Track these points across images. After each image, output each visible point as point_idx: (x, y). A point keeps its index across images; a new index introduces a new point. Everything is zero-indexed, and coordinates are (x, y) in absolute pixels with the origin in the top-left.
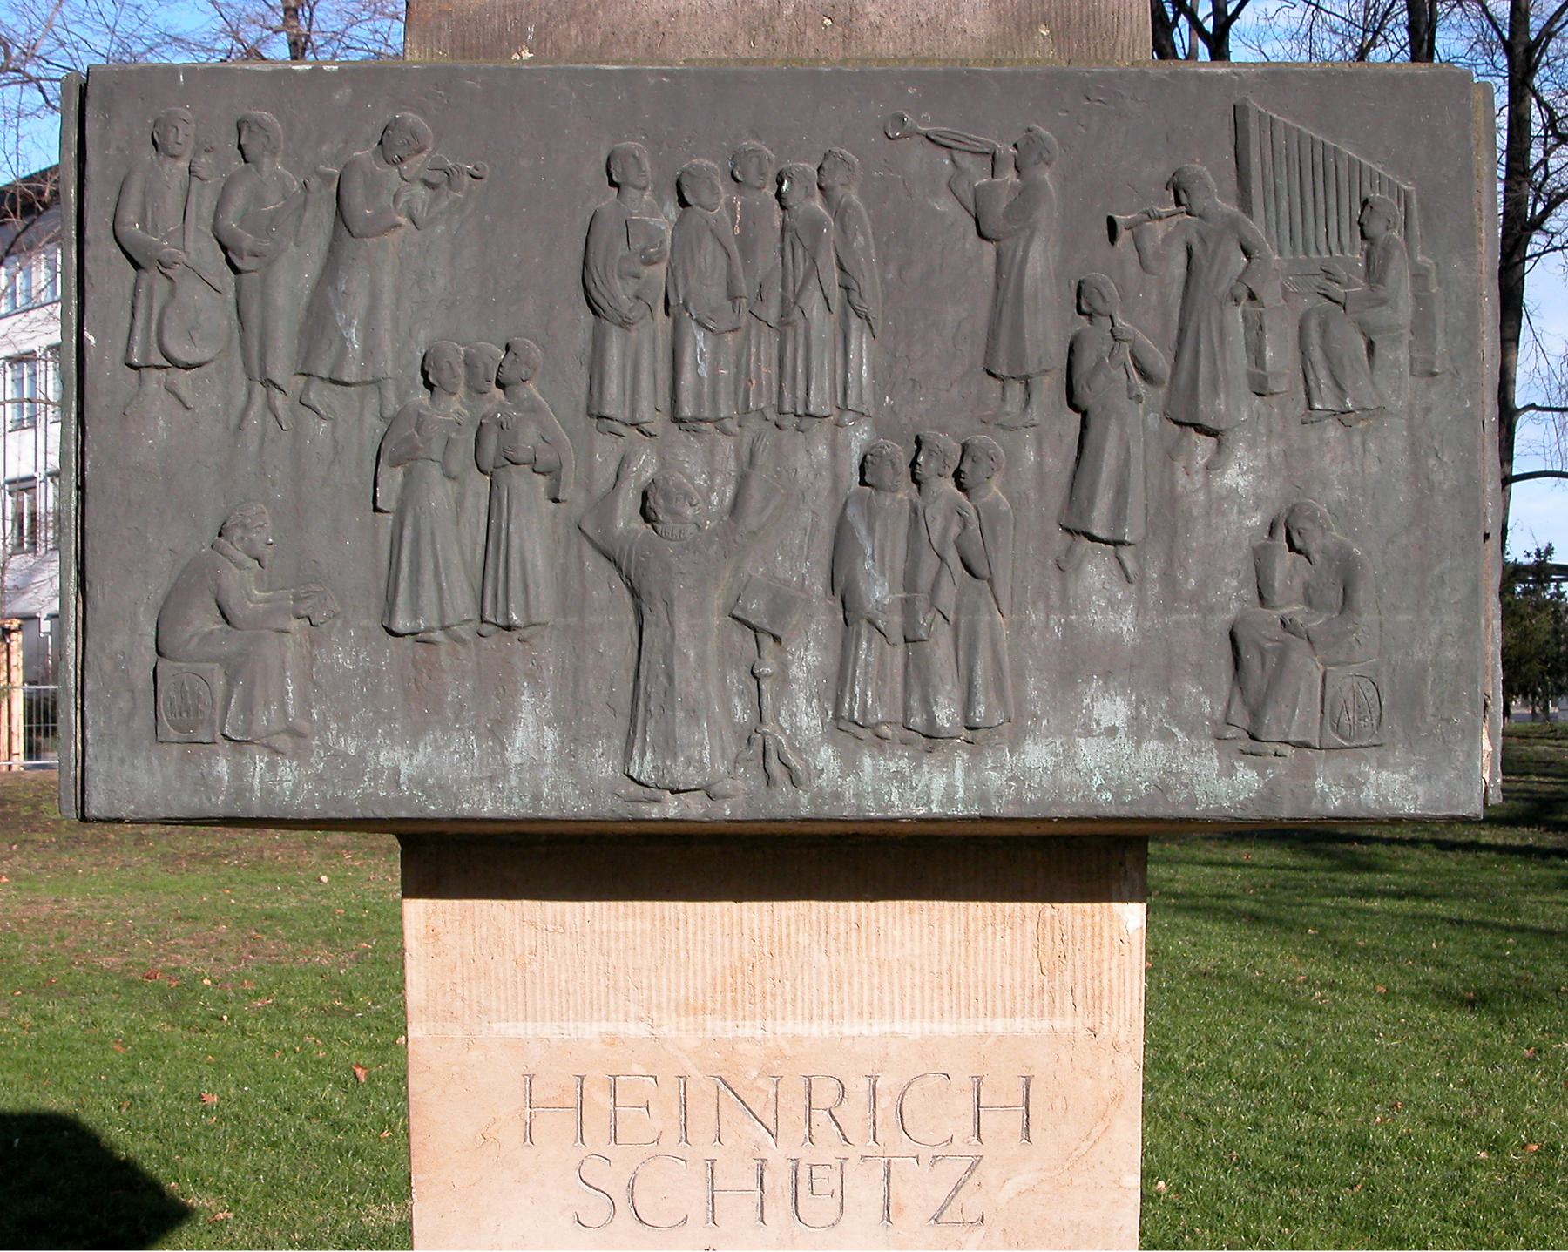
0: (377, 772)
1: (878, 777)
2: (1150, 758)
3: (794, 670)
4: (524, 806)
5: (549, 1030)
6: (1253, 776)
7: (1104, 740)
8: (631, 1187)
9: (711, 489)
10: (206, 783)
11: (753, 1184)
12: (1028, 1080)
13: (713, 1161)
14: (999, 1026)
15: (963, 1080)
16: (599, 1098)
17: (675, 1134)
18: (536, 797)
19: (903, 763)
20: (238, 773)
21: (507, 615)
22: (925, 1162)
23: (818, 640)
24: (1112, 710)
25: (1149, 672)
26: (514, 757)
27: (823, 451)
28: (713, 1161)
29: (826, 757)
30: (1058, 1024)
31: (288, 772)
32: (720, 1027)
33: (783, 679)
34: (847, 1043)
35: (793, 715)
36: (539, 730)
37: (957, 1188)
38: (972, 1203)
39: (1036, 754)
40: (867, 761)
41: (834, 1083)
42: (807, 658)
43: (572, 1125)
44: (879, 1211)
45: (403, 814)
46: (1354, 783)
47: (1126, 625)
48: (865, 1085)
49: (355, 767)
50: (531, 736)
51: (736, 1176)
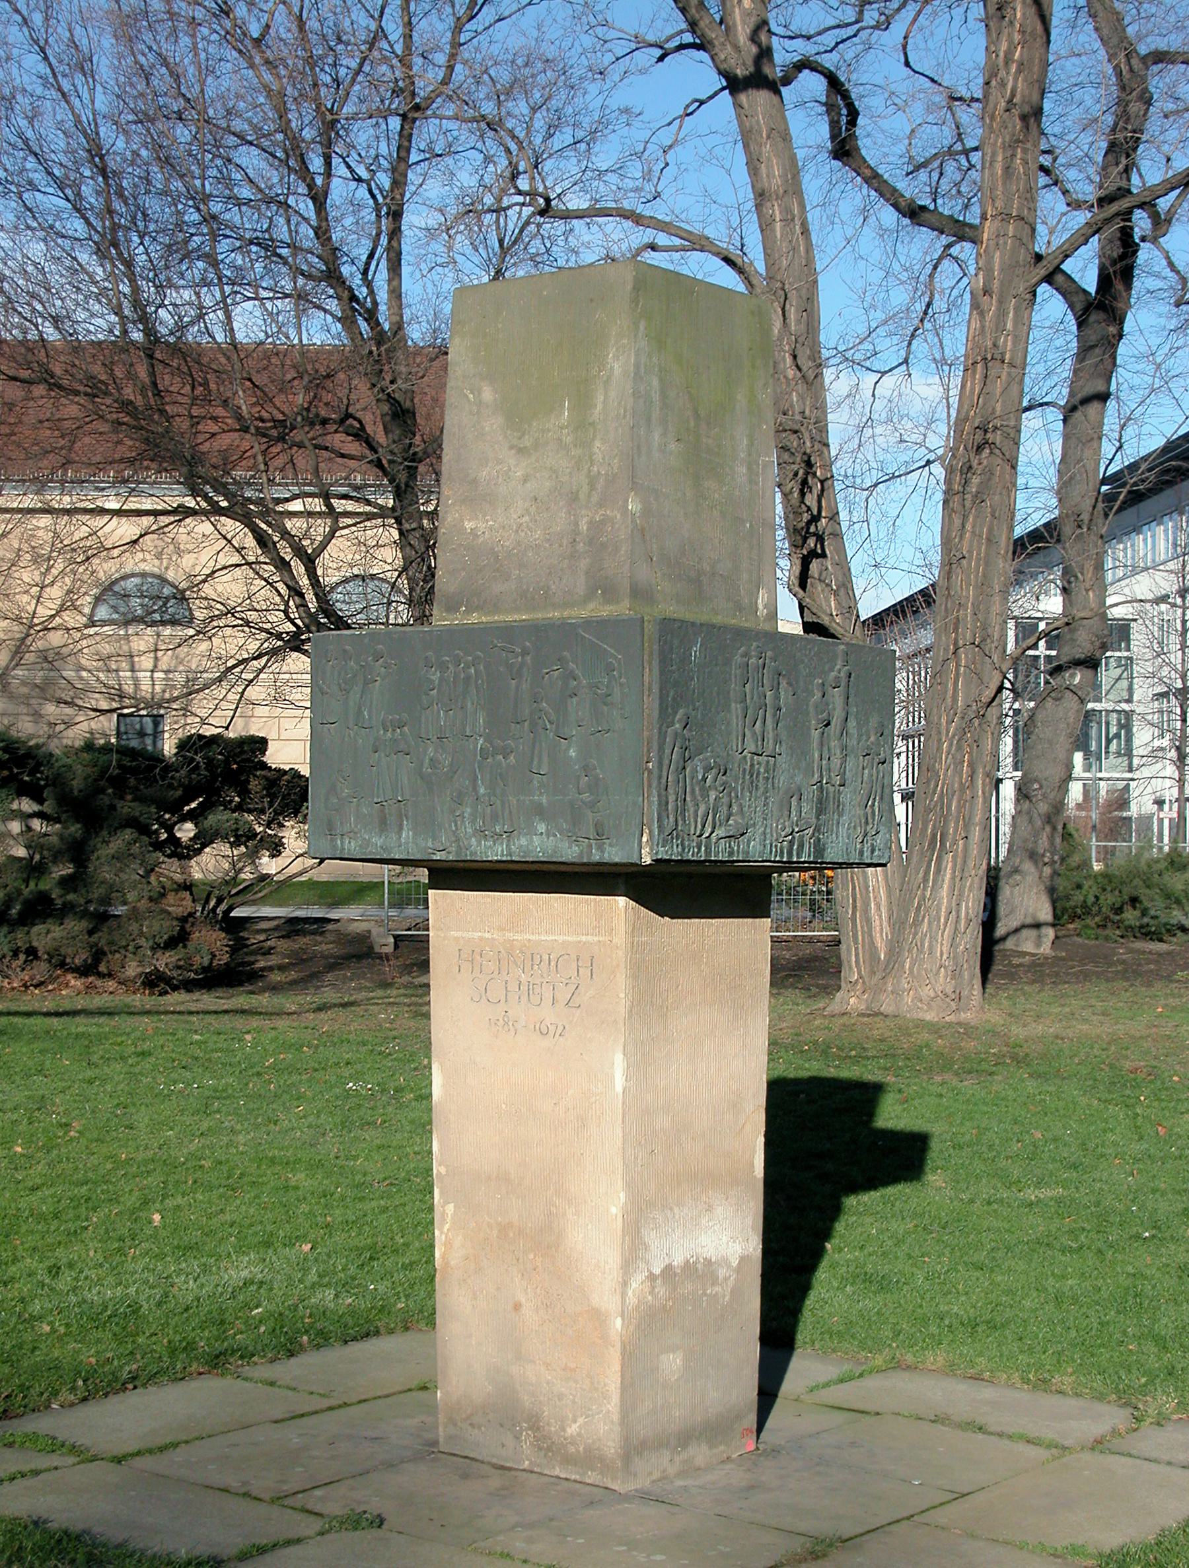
5: (465, 935)
8: (669, 124)
10: (335, 847)
14: (584, 938)
15: (574, 957)
32: (509, 935)
49: (367, 843)
51: (513, 986)
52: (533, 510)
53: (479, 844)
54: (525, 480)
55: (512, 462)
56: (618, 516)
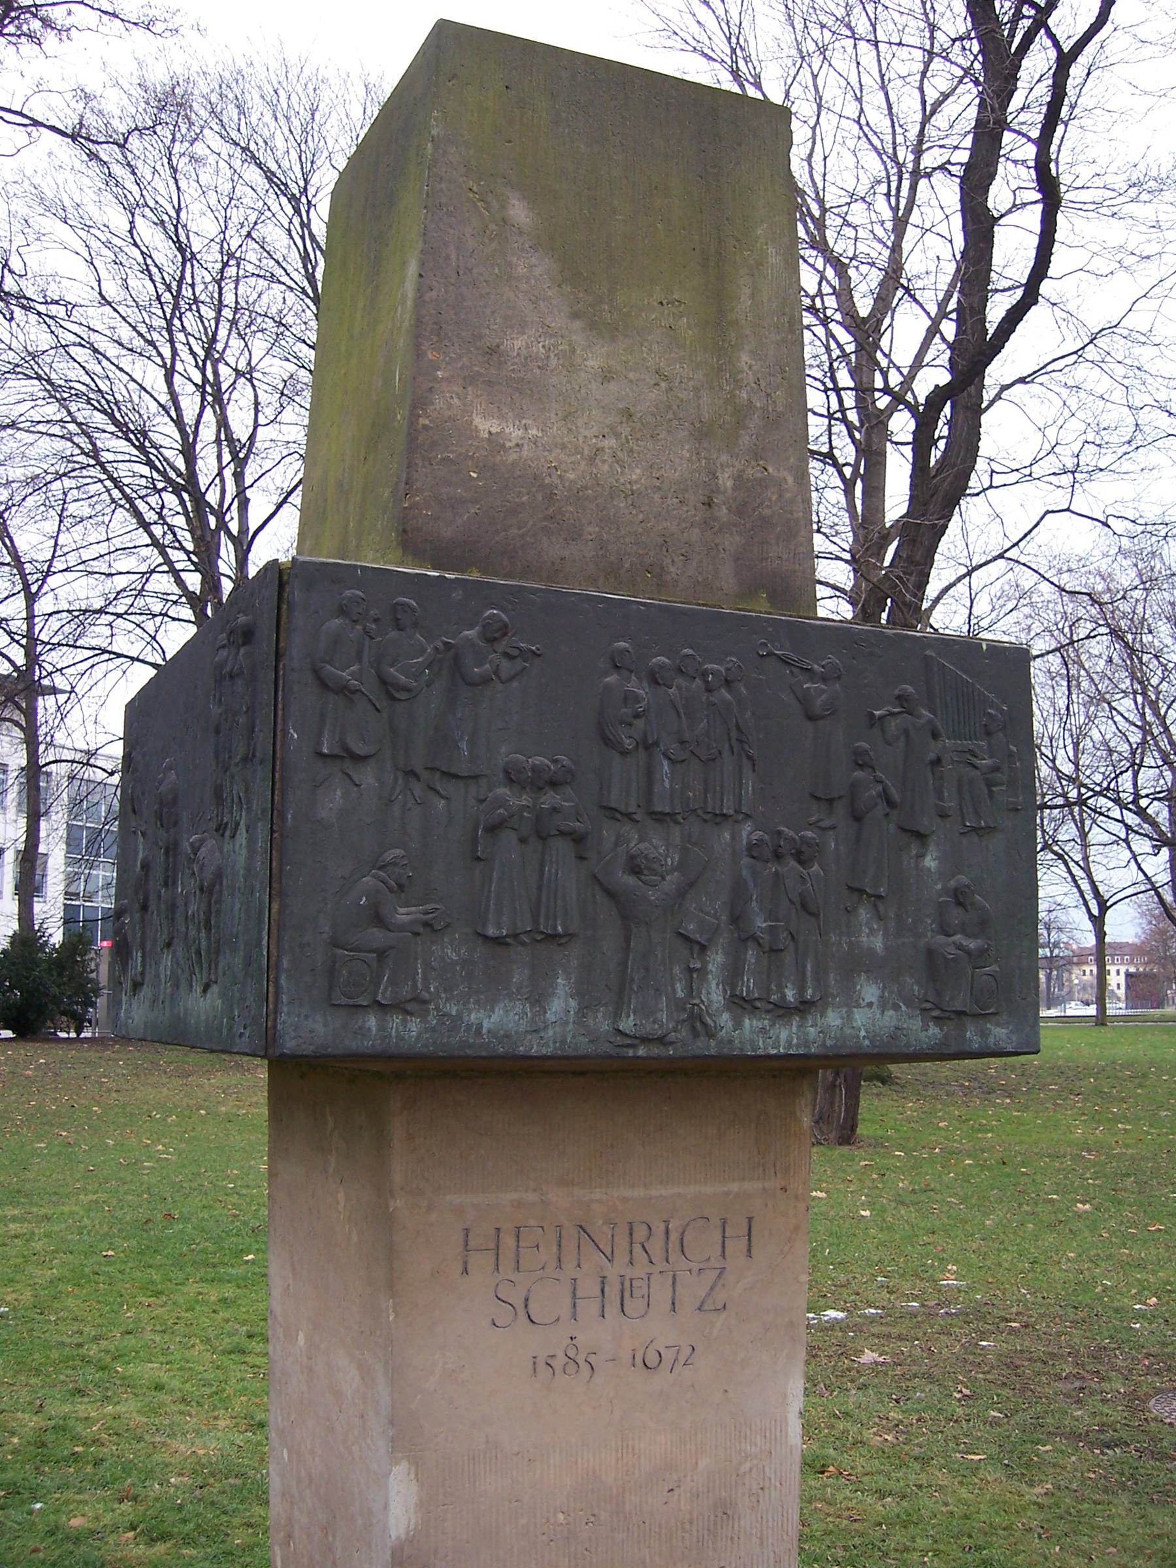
0: (469, 1027)
1: (752, 1031)
2: (889, 1019)
3: (710, 967)
4: (555, 1049)
6: (937, 1030)
7: (866, 1009)
8: (527, 1300)
9: (667, 856)
10: (363, 1032)
11: (599, 1293)
12: (750, 1219)
13: (575, 1280)
15: (715, 1221)
16: (509, 1241)
17: (553, 1263)
18: (563, 1042)
19: (766, 1022)
20: (382, 1028)
21: (555, 928)
22: (695, 1271)
23: (723, 948)
24: (870, 992)
25: (883, 968)
26: (550, 1017)
27: (727, 836)
28: (575, 1280)
29: (725, 1018)
30: (767, 1185)
31: (415, 1025)
33: (703, 972)
34: (654, 1201)
35: (709, 993)
36: (566, 1002)
37: (712, 1289)
38: (720, 1297)
39: (833, 1018)
40: (747, 1021)
41: (645, 1227)
42: (716, 960)
43: (492, 1260)
44: (669, 1306)
45: (484, 1054)
46: (984, 1034)
47: (878, 943)
48: (662, 1227)
50: (561, 1004)
52: (625, 430)
53: (738, 1025)
54: (607, 376)
55: (579, 339)
56: (790, 479)
